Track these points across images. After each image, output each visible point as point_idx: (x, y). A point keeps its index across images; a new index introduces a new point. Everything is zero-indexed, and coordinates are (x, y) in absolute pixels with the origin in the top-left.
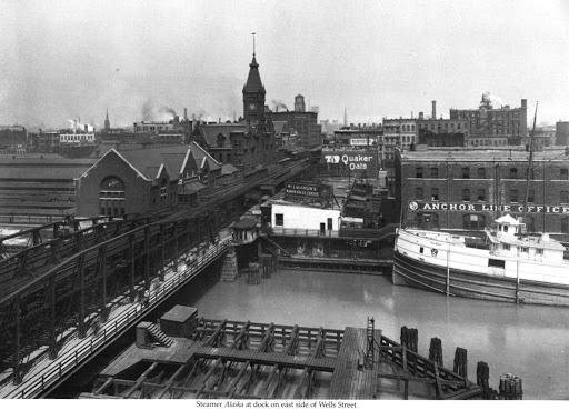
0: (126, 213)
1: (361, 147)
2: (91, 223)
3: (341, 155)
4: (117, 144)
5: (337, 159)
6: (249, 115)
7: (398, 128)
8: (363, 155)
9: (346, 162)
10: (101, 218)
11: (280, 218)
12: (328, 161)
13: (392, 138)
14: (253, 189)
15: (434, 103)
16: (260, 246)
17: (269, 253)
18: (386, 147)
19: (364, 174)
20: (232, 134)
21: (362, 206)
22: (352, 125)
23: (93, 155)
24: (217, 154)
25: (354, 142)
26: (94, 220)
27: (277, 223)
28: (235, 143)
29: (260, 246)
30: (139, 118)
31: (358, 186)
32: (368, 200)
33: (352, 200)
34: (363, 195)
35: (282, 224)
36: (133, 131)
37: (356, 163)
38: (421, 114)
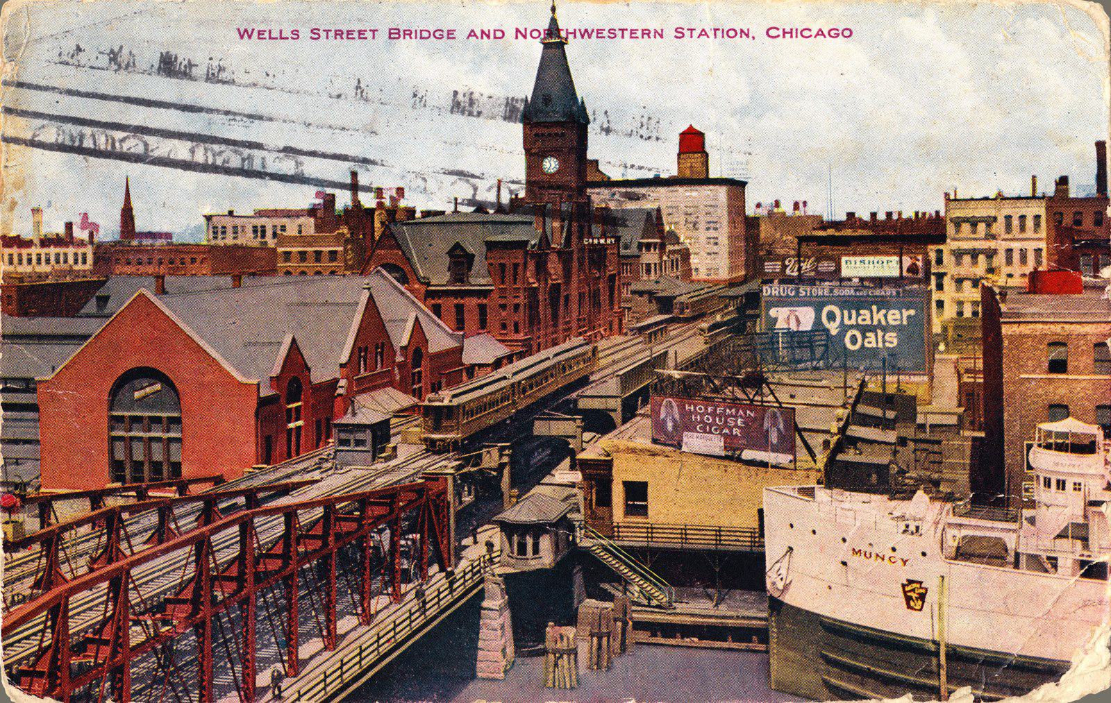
0: (187, 471)
1: (880, 282)
2: (87, 503)
3: (868, 296)
4: (160, 278)
5: (806, 318)
6: (538, 539)
7: (989, 221)
8: (883, 304)
9: (833, 328)
10: (111, 492)
11: (637, 492)
12: (780, 325)
13: (974, 254)
14: (638, 199)
15: (1034, 177)
16: (578, 580)
17: (608, 597)
18: (959, 281)
19: (890, 362)
20: (491, 246)
21: (884, 460)
22: (851, 215)
23: (91, 306)
24: (449, 303)
25: (855, 267)
26: (96, 498)
27: (630, 510)
28: (500, 272)
29: (578, 580)
30: (166, 155)
31: (873, 399)
32: (902, 441)
33: (854, 441)
34: (886, 424)
35: (643, 511)
36: (204, 239)
37: (864, 330)
38: (1063, 181)
